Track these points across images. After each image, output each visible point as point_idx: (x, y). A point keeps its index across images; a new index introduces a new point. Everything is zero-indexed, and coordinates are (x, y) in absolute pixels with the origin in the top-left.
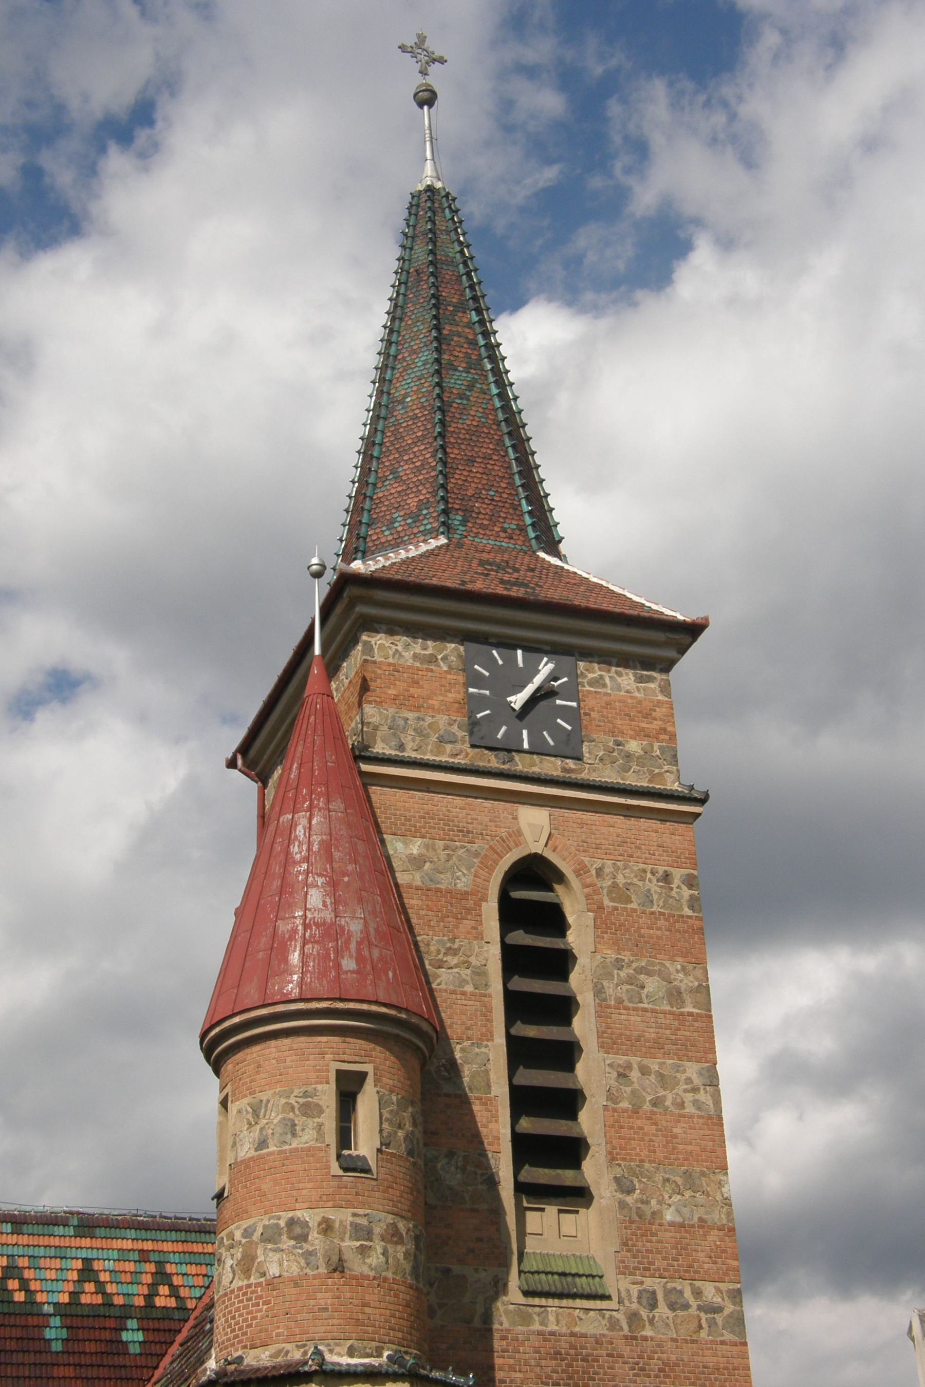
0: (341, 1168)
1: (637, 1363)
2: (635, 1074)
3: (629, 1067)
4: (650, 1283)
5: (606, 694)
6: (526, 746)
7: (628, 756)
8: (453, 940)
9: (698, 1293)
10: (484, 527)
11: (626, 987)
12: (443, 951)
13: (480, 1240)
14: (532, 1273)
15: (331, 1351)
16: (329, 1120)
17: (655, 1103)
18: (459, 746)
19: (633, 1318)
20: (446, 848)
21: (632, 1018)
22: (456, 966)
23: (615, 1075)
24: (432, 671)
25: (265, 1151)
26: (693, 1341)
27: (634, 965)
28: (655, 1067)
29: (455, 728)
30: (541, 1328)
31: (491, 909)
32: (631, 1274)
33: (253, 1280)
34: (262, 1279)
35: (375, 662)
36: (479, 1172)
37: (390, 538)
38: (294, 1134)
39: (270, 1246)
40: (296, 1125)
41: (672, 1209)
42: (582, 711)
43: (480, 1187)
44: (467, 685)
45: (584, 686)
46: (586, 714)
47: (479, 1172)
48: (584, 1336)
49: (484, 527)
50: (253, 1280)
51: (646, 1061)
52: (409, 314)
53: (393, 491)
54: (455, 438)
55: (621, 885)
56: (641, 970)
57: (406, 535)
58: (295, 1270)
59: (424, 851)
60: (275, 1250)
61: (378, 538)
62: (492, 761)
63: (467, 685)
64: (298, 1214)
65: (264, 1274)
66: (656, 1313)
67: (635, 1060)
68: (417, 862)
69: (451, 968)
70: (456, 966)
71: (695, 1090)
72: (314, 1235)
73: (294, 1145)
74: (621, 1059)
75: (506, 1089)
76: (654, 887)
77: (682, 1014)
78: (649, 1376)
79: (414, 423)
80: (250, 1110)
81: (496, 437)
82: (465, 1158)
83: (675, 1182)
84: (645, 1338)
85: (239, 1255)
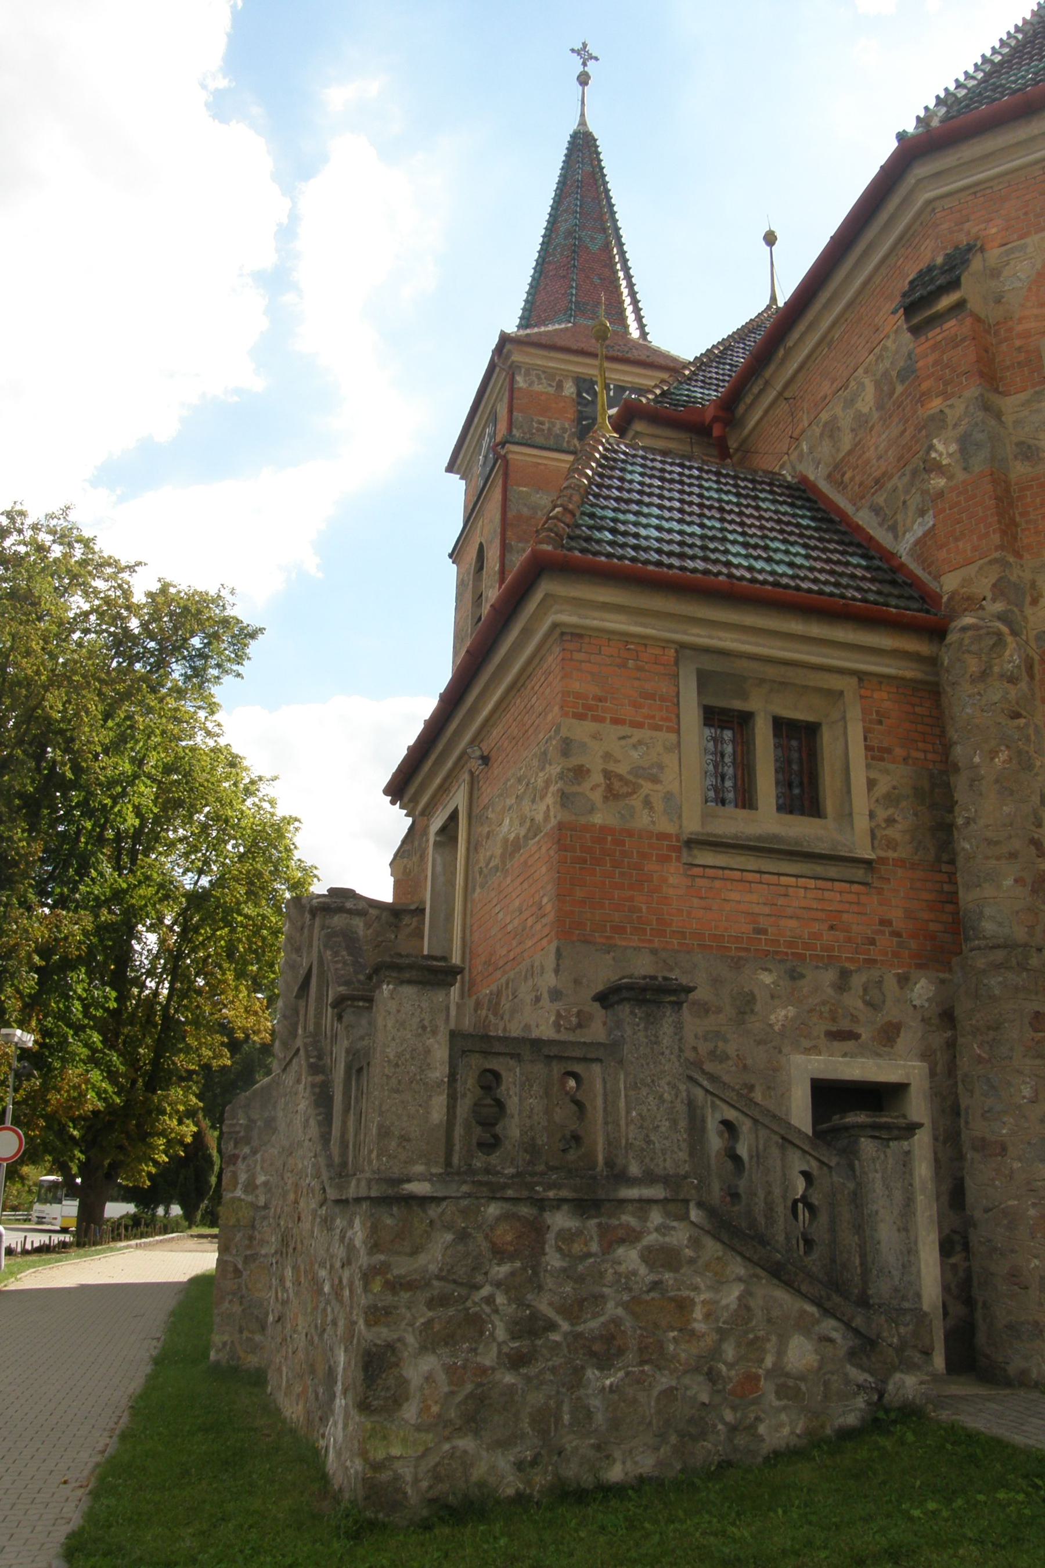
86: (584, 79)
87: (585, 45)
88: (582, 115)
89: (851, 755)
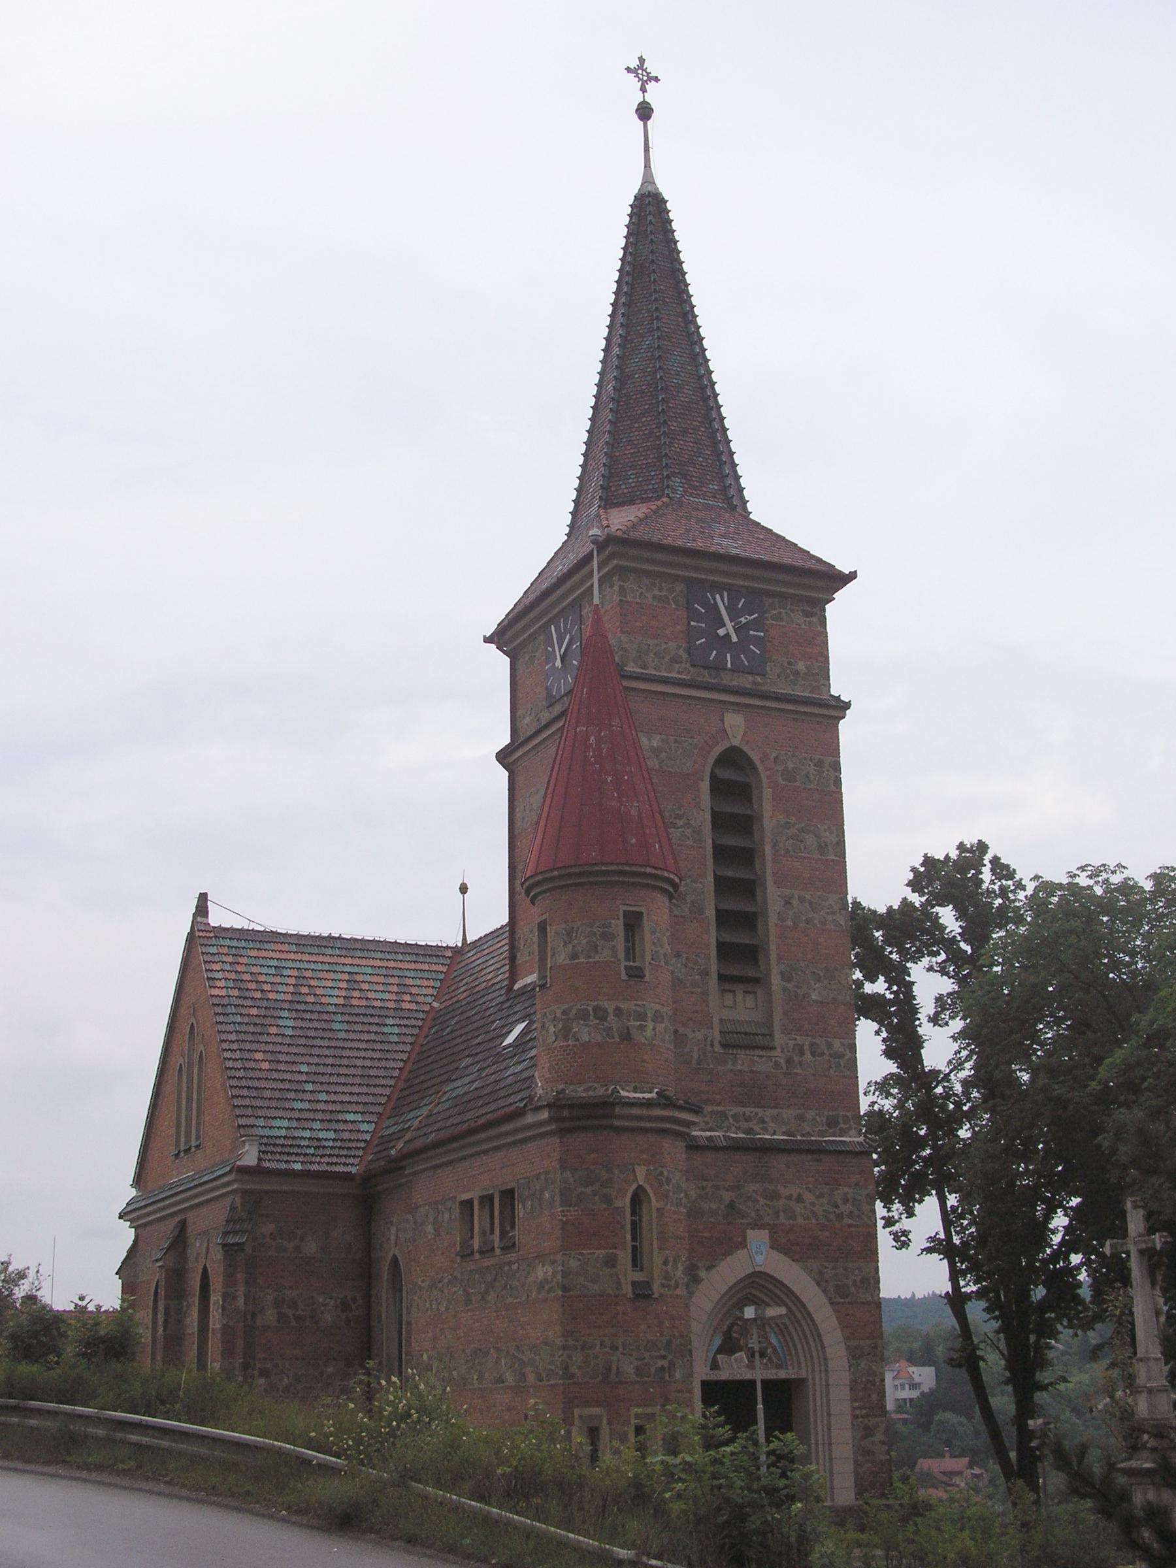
0: (627, 974)
1: (790, 1090)
2: (795, 902)
3: (792, 897)
4: (800, 1039)
5: (783, 626)
6: (729, 665)
7: (797, 673)
8: (679, 808)
9: (829, 1046)
10: (696, 488)
11: (791, 841)
12: (673, 816)
13: (696, 1012)
14: (729, 1033)
15: (623, 1089)
16: (620, 943)
17: (808, 922)
18: (684, 665)
19: (789, 1061)
20: (676, 741)
21: (795, 864)
22: (682, 827)
23: (782, 903)
24: (665, 608)
25: (576, 961)
26: (825, 1076)
27: (797, 827)
28: (808, 897)
29: (681, 652)
30: (732, 1067)
31: (705, 785)
32: (789, 1034)
33: (570, 1042)
34: (577, 1043)
35: (627, 602)
36: (696, 967)
37: (625, 491)
38: (597, 952)
39: (582, 1022)
40: (597, 946)
41: (816, 992)
42: (766, 639)
43: (697, 977)
44: (689, 619)
45: (768, 620)
46: (769, 641)
47: (696, 967)
48: (759, 1072)
49: (696, 488)
50: (570, 1042)
51: (803, 893)
52: (635, 301)
53: (627, 452)
54: (673, 413)
55: (790, 769)
56: (802, 830)
57: (638, 490)
58: (599, 1039)
59: (660, 744)
60: (586, 1025)
61: (616, 490)
62: (706, 677)
63: (689, 619)
64: (601, 1003)
65: (578, 1040)
66: (804, 1058)
67: (796, 893)
68: (656, 752)
69: (678, 828)
70: (682, 827)
71: (833, 913)
72: (611, 1017)
73: (597, 959)
74: (788, 892)
75: (714, 912)
76: (812, 769)
77: (827, 860)
78: (797, 1097)
79: (642, 397)
80: (565, 933)
81: (703, 412)
82: (687, 958)
83: (819, 974)
84: (796, 1074)
85: (560, 1026)
86: (645, 112)
87: (642, 60)
88: (647, 165)
89: (467, 934)
